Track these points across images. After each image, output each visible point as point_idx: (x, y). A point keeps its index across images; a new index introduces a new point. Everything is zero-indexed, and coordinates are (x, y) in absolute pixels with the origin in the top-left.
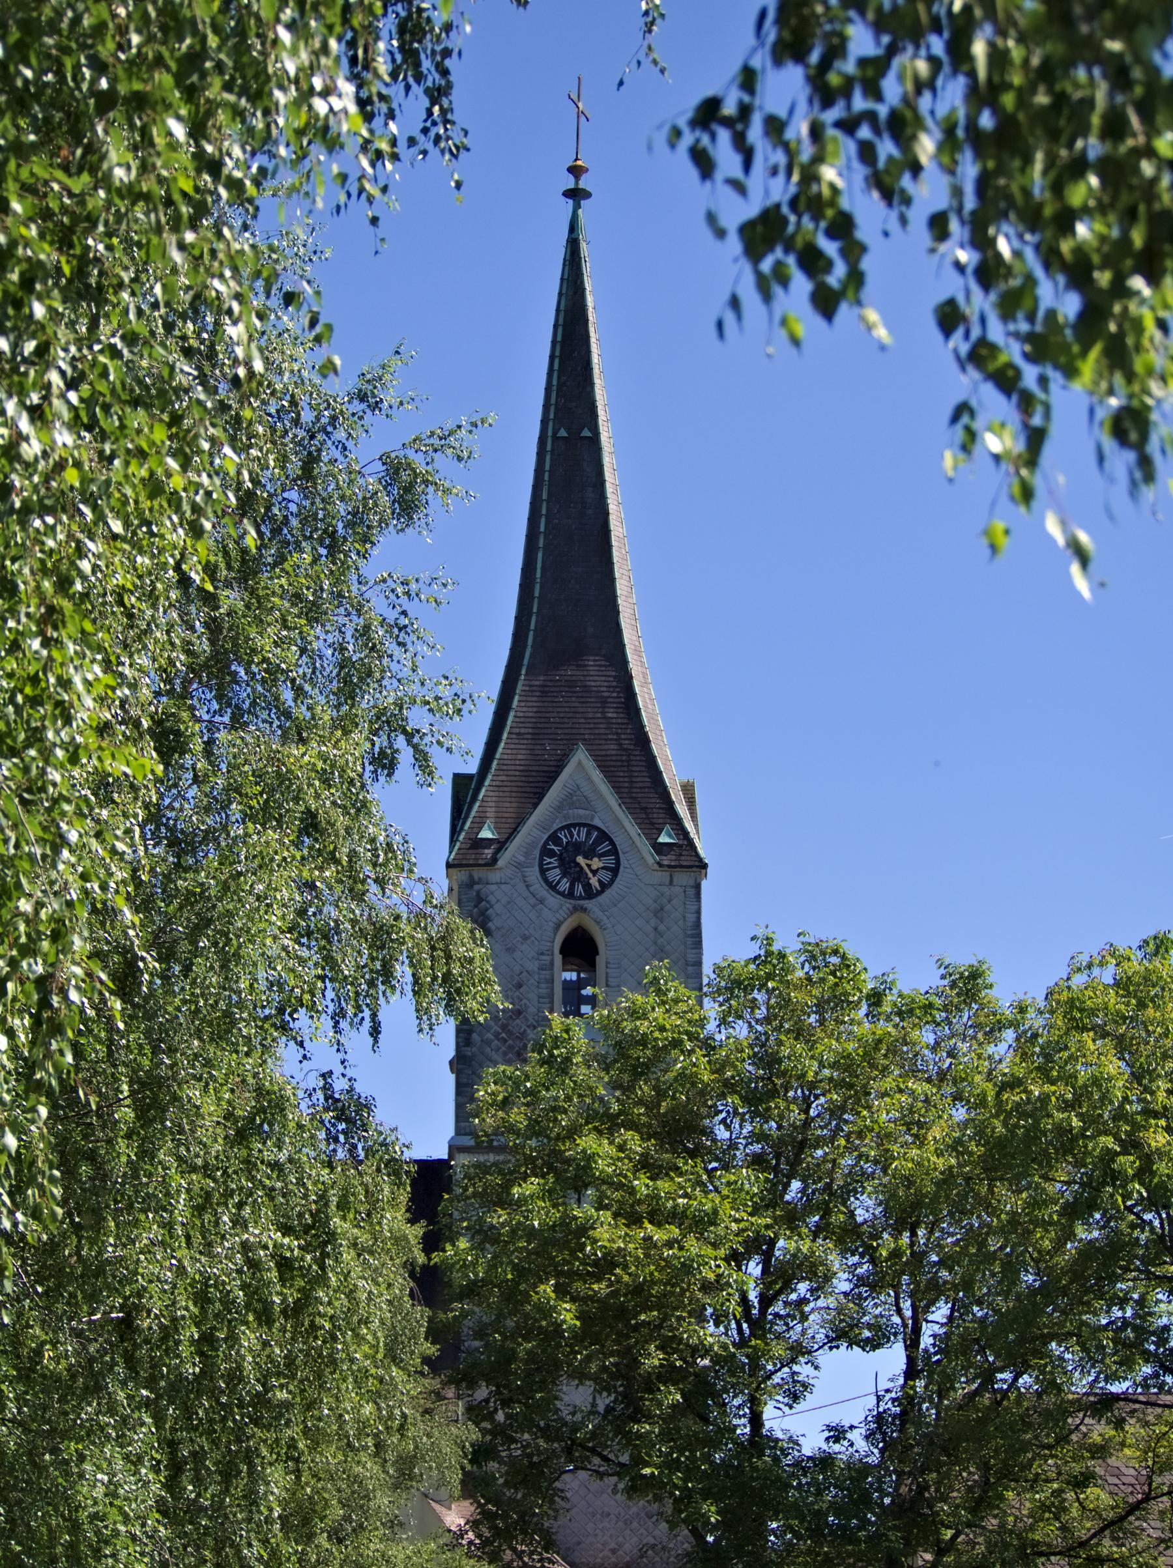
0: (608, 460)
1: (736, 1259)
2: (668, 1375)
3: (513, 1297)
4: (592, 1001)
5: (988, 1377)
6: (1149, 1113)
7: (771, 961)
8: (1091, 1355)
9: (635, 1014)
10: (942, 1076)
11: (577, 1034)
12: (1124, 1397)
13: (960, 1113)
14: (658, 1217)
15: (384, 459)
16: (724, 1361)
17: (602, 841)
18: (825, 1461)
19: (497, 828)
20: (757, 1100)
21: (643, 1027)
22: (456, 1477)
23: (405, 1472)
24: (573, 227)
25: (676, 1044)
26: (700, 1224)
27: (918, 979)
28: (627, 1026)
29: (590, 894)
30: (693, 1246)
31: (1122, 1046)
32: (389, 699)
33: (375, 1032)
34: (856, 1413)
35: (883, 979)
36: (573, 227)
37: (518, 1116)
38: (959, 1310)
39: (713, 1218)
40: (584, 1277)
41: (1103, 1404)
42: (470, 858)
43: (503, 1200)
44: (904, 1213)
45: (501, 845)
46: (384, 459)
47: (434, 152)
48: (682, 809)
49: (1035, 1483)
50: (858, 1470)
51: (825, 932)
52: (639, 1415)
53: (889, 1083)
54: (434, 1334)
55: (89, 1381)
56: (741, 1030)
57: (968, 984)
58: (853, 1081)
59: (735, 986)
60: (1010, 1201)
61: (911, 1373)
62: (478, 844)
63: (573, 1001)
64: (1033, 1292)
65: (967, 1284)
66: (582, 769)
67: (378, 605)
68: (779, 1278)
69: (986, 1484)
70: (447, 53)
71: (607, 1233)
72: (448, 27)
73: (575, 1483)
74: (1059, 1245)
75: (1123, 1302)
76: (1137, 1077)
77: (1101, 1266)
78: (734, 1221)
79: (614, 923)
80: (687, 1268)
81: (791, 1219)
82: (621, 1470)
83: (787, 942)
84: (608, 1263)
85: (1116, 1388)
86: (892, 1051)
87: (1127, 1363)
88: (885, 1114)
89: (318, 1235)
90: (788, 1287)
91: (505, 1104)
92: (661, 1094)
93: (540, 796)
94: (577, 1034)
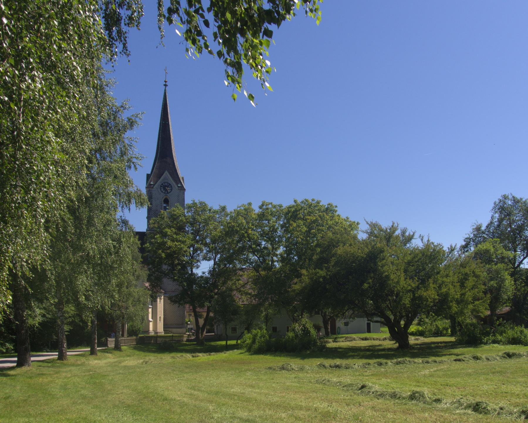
0: (171, 127)
1: (189, 247)
2: (179, 264)
3: (155, 252)
4: (168, 209)
5: (225, 265)
6: (249, 228)
7: (194, 204)
8: (240, 263)
9: (174, 211)
10: (219, 222)
11: (165, 213)
12: (245, 268)
13: (222, 227)
14: (177, 241)
15: (128, 118)
16: (187, 262)
17: (170, 185)
18: (202, 277)
19: (153, 182)
20: (192, 224)
21: (175, 213)
22: (146, 279)
23: (138, 278)
24: (165, 90)
25: (180, 216)
26: (183, 242)
27: (216, 207)
28: (173, 213)
29: (168, 193)
30: (182, 245)
31: (245, 218)
32: (129, 157)
33: (129, 210)
34: (206, 270)
35: (211, 207)
36: (165, 90)
37: (156, 226)
38: (222, 256)
39: (185, 241)
40: (166, 249)
41: (242, 269)
42: (149, 187)
43: (154, 238)
44: (214, 241)
45: (154, 185)
46: (128, 118)
47: (124, 55)
48: (182, 181)
49: (232, 280)
50: (207, 278)
51: (202, 200)
52: (174, 270)
53: (212, 223)
54: (142, 257)
55: (79, 264)
56: (190, 214)
57: (223, 209)
58: (206, 222)
59: (189, 207)
60: (229, 240)
61: (214, 264)
62: (151, 185)
63: (165, 209)
64: (232, 253)
65: (223, 252)
66: (166, 174)
67: (126, 141)
68: (195, 251)
69: (225, 281)
70: (126, 37)
71: (169, 243)
72: (126, 32)
73: (165, 280)
74: (236, 247)
75: (245, 255)
76: (247, 223)
77: (243, 249)
78: (189, 242)
79: (172, 197)
80: (181, 249)
81: (197, 242)
82: (172, 278)
83: (197, 201)
84: (170, 247)
85: (244, 267)
86: (212, 218)
87: (245, 264)
88: (211, 227)
89: (119, 241)
90: (197, 252)
91: (154, 223)
92: (178, 223)
93: (160, 178)
94: (165, 213)
